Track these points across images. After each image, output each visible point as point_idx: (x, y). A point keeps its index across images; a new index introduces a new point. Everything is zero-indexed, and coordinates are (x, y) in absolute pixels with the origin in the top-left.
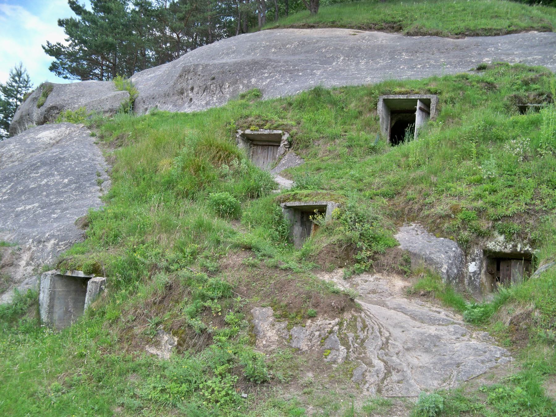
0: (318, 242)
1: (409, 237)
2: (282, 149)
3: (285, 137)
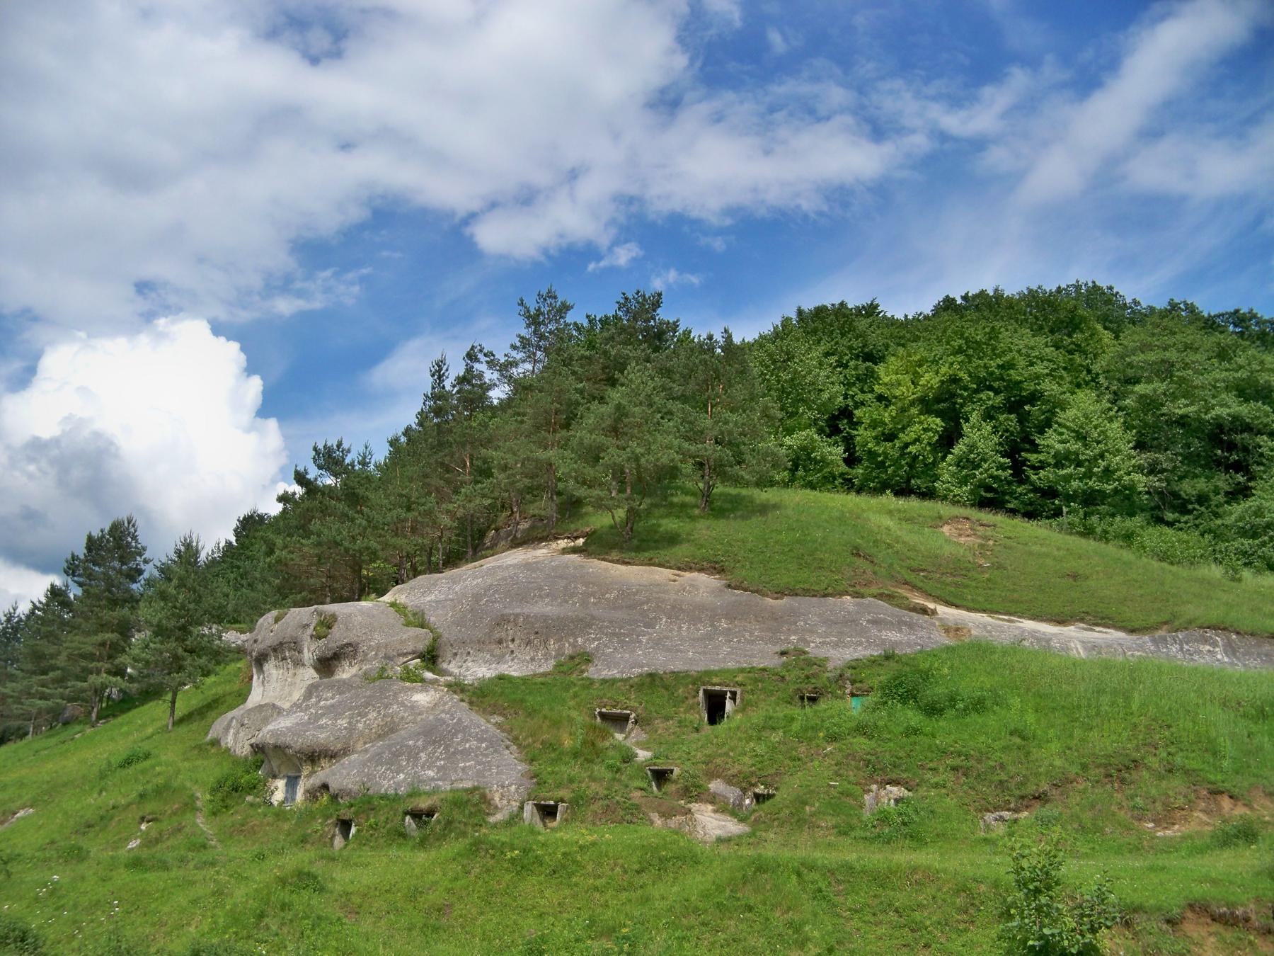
0: (670, 788)
1: (716, 786)
2: (630, 725)
3: (633, 716)
